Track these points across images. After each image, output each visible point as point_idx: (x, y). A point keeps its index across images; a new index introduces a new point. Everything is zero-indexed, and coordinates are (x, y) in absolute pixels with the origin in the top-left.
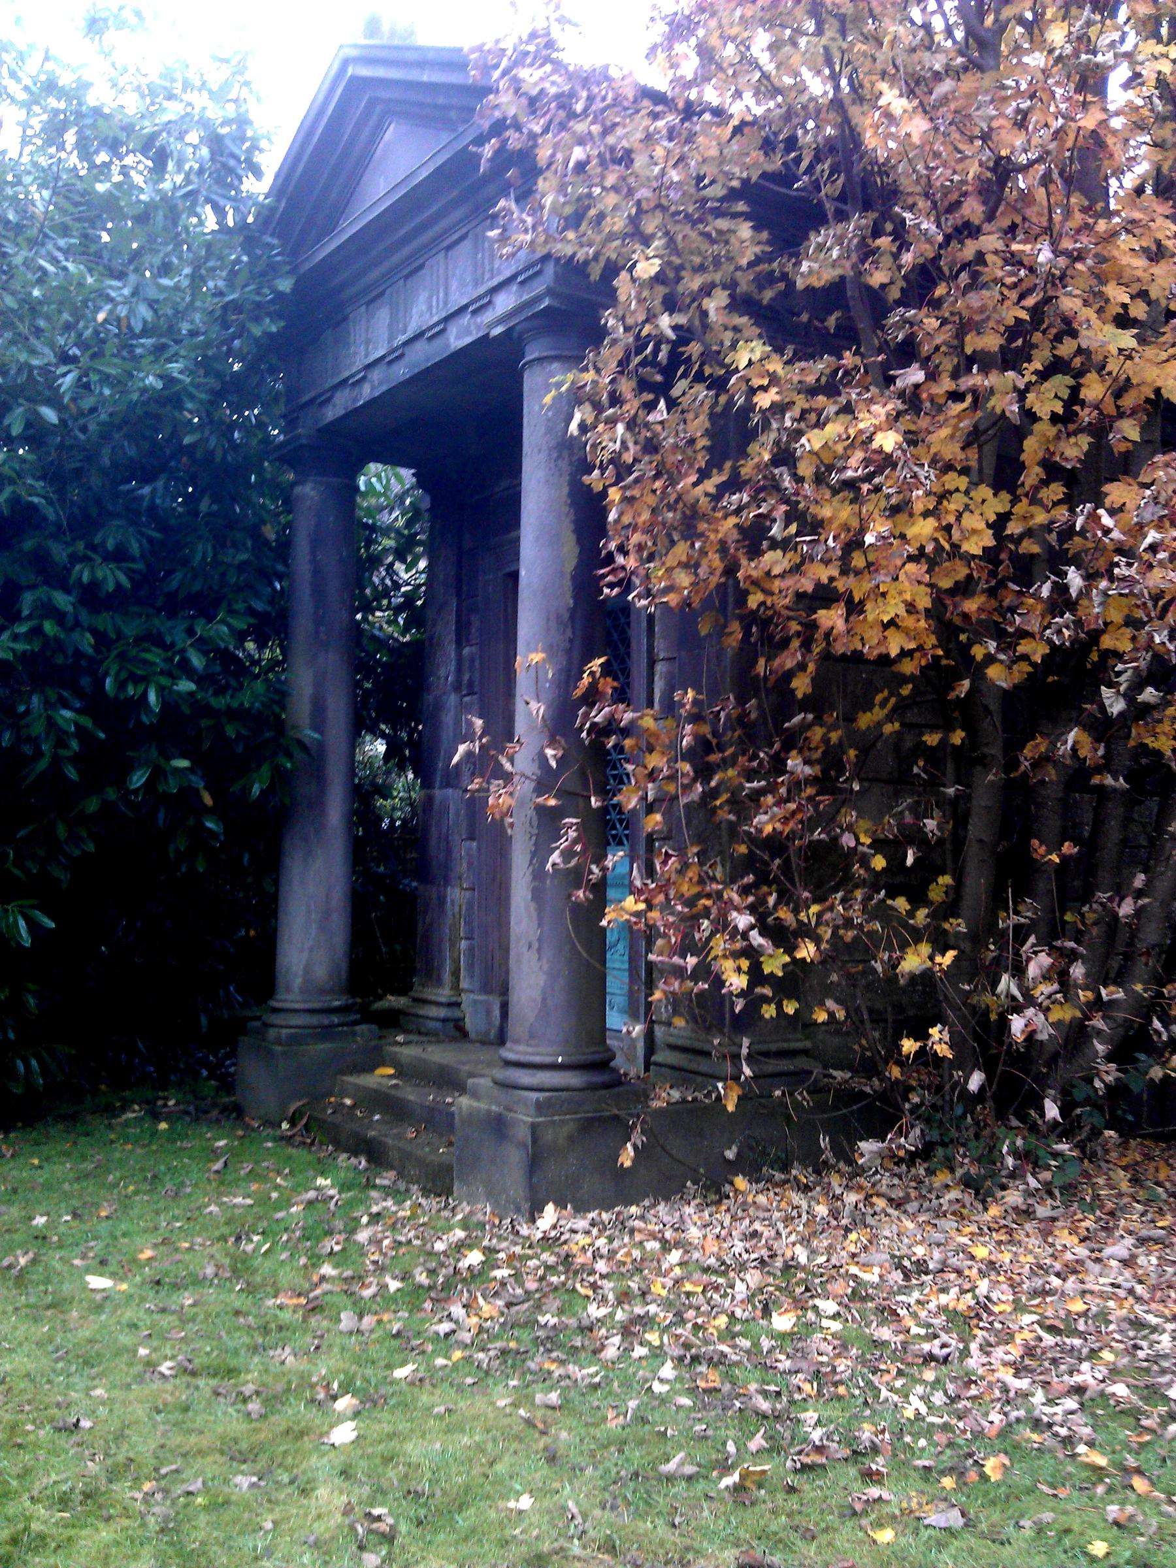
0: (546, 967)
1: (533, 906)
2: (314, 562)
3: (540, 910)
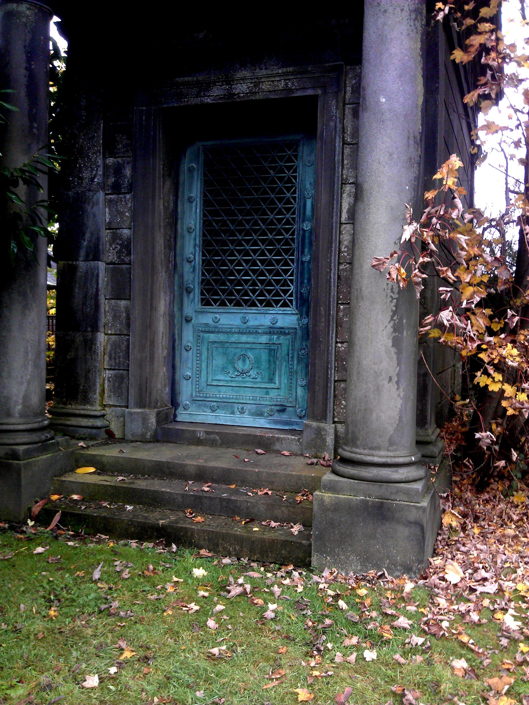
0: (402, 394)
1: (393, 350)
2: (28, 69)
3: (399, 353)
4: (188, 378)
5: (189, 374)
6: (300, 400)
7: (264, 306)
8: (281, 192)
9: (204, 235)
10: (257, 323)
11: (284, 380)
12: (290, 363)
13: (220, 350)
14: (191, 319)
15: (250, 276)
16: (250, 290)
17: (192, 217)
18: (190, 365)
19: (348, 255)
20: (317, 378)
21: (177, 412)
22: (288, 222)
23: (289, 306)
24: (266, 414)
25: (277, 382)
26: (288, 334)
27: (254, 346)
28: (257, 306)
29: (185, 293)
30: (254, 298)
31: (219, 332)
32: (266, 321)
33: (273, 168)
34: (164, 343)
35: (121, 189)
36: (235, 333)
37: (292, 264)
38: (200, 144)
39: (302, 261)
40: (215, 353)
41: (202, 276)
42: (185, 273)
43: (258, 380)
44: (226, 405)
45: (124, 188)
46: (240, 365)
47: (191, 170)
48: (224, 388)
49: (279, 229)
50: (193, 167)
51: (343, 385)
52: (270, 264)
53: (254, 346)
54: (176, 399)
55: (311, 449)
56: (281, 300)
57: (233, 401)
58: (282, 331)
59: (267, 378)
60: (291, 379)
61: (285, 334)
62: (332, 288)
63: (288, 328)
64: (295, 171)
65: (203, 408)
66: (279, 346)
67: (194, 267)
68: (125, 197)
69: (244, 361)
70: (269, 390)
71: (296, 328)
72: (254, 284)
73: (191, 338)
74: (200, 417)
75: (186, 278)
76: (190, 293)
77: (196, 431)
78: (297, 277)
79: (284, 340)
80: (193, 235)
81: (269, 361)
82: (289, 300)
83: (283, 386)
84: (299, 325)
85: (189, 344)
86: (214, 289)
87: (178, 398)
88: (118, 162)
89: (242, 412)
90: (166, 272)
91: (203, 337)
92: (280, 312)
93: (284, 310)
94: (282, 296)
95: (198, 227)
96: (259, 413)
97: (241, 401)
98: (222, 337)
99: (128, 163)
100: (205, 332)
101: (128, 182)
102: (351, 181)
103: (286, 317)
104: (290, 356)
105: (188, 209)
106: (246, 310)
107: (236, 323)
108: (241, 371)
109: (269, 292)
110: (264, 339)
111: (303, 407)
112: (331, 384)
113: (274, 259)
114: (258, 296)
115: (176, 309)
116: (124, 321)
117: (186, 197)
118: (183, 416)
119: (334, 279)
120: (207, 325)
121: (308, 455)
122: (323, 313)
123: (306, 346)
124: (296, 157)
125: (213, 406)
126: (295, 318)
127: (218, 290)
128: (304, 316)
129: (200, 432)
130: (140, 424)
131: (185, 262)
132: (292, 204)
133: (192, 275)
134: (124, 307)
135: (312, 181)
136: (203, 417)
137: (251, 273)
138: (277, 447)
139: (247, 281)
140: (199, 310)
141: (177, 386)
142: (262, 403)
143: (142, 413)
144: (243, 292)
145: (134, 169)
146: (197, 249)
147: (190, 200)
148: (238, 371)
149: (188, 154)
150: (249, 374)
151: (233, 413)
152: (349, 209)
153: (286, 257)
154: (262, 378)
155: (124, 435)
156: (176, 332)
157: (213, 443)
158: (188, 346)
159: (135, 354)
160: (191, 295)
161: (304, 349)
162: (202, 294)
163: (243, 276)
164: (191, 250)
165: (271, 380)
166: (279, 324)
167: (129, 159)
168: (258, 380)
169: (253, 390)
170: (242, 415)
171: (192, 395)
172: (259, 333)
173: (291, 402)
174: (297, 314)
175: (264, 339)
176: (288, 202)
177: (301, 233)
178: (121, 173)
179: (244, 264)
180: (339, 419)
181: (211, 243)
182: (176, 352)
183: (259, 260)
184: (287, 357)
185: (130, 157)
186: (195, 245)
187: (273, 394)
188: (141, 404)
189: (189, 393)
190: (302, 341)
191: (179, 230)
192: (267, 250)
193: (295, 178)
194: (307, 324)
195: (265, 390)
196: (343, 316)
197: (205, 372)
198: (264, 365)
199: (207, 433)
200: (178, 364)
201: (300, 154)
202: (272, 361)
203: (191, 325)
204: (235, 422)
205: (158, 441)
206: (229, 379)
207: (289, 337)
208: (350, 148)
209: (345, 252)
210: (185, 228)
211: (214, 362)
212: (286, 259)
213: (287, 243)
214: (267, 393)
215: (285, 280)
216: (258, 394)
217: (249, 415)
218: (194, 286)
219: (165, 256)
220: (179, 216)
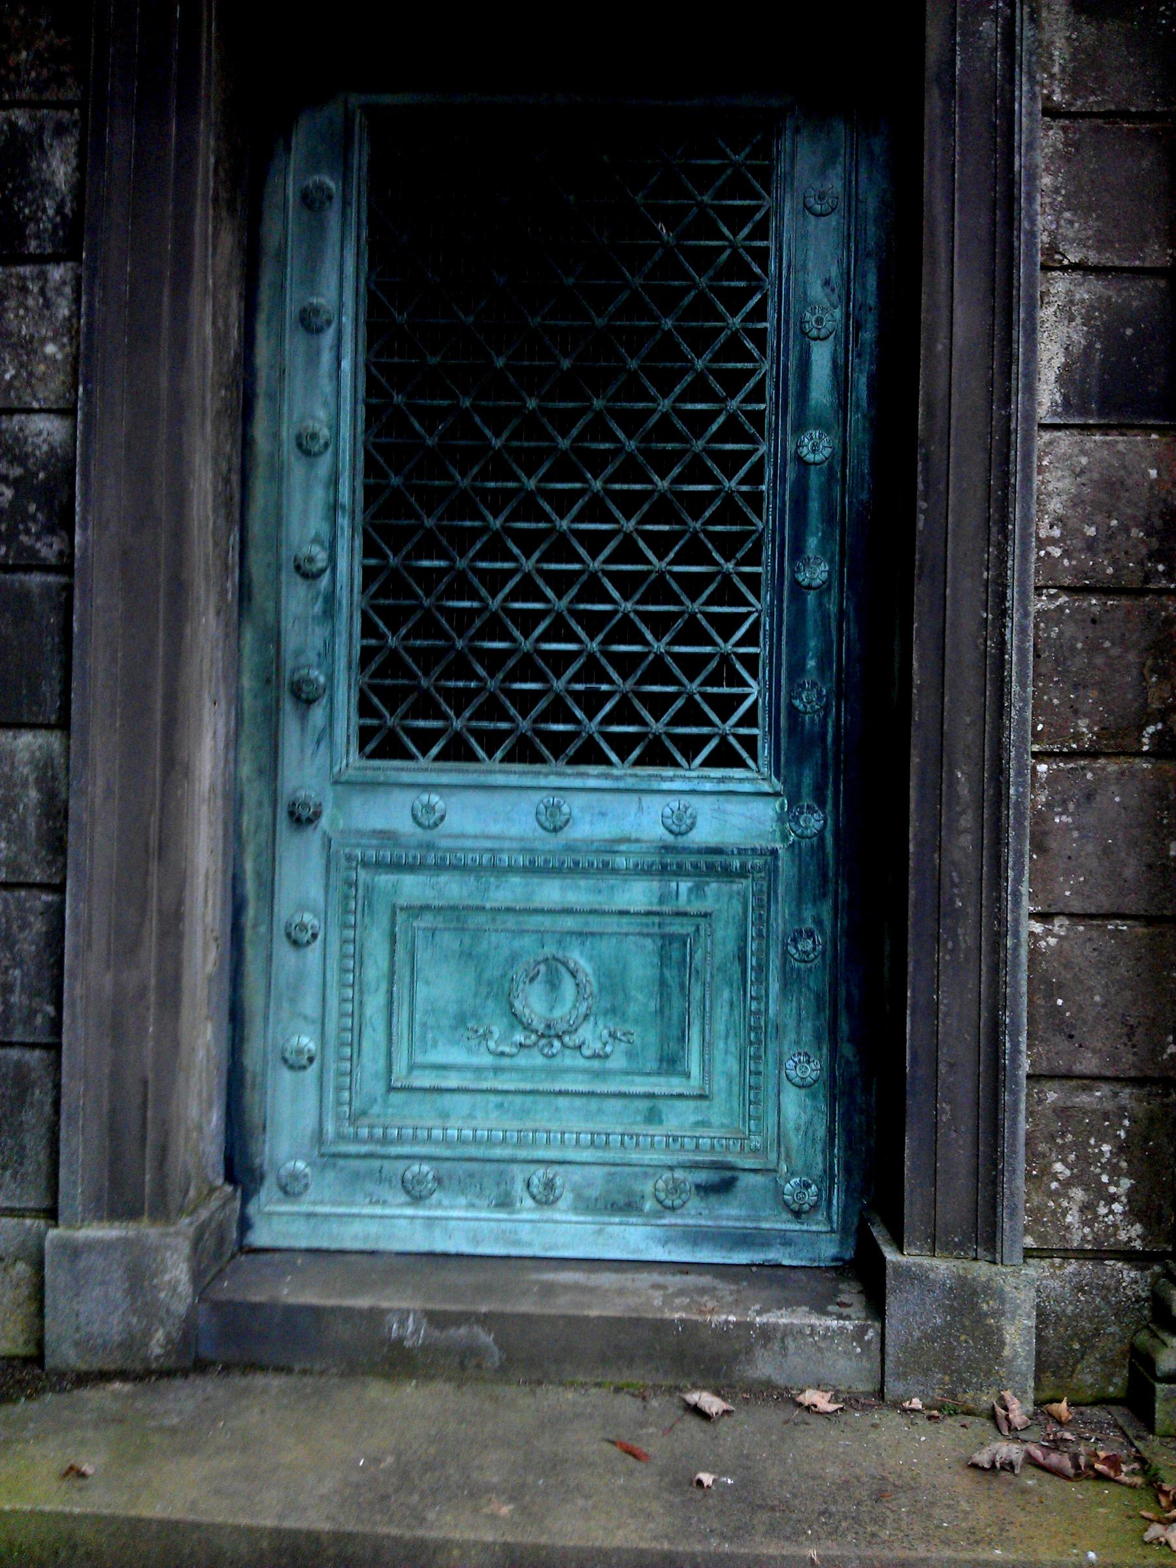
4: (296, 1064)
5: (307, 1042)
6: (795, 1140)
7: (639, 762)
8: (701, 307)
9: (371, 467)
10: (604, 830)
11: (726, 1063)
12: (752, 990)
13: (448, 940)
14: (317, 815)
15: (573, 638)
16: (575, 695)
17: (321, 393)
18: (309, 1004)
19: (1066, 553)
20: (943, 1069)
21: (252, 1209)
22: (732, 430)
23: (742, 764)
24: (648, 1205)
25: (695, 1070)
26: (743, 873)
27: (595, 923)
28: (608, 762)
29: (288, 705)
30: (593, 726)
31: (440, 867)
32: (645, 820)
33: (672, 218)
34: (209, 919)
35: (23, 240)
36: (511, 869)
37: (751, 598)
38: (355, 100)
39: (795, 583)
40: (423, 956)
41: (365, 634)
42: (287, 624)
43: (611, 1064)
44: (480, 1173)
45: (37, 236)
46: (534, 1003)
47: (312, 201)
48: (466, 1098)
49: (697, 457)
50: (320, 187)
51: (1052, 1096)
52: (659, 590)
53: (595, 923)
54: (245, 1153)
55: (926, 1372)
56: (707, 739)
57: (506, 1152)
58: (714, 864)
59: (652, 1053)
60: (757, 1058)
61: (727, 873)
62: (1015, 688)
63: (741, 852)
64: (761, 231)
65: (369, 1186)
66: (702, 922)
67: (330, 599)
68: (43, 276)
69: (553, 985)
70: (662, 1105)
71: (774, 852)
72: (592, 670)
73: (315, 891)
74: (357, 1227)
75: (291, 640)
76: (309, 702)
77: (383, 1312)
78: (775, 649)
79: (720, 899)
80: (324, 465)
81: (663, 983)
82: (738, 737)
83: (719, 1083)
84: (785, 837)
85: (308, 918)
86: (418, 687)
87: (253, 1148)
88: (12, 125)
89: (546, 1197)
90: (218, 613)
91: (370, 889)
92: (708, 786)
93: (722, 780)
94: (711, 724)
95: (346, 431)
96: (621, 1200)
97: (540, 1154)
98: (453, 889)
99: (60, 130)
100: (379, 865)
101: (59, 209)
102: (1073, 258)
103: (734, 807)
104: (752, 961)
105: (300, 361)
106: (554, 776)
107: (514, 831)
108: (541, 1028)
109: (657, 705)
110: (638, 894)
111: (808, 1167)
112: (1015, 1093)
113: (677, 576)
114: (607, 720)
115: (246, 770)
116: (32, 823)
117: (292, 309)
118: (278, 1225)
119: (1022, 652)
120: (387, 836)
121: (917, 1403)
122: (964, 791)
123: (818, 922)
124: (766, 176)
125: (419, 1179)
126: (767, 811)
127: (437, 688)
128: (806, 801)
129: (403, 1316)
130: (117, 1294)
131: (288, 576)
132: (752, 359)
133: (322, 632)
134: (32, 760)
135: (834, 271)
136: (373, 1228)
137: (579, 630)
138: (764, 1367)
139: (560, 661)
140: (351, 774)
141: (251, 1098)
142: (634, 1156)
143: (126, 1241)
144: (542, 705)
145: (89, 159)
146: (344, 522)
147: (310, 322)
148: (527, 1028)
149: (299, 139)
150: (576, 1039)
151: (505, 1203)
152: (1066, 367)
153: (730, 566)
154: (630, 1055)
155: (40, 1344)
156: (249, 866)
157: (463, 1365)
158: (303, 927)
159: (88, 977)
160: (318, 714)
161: (810, 934)
162: (365, 708)
163: (546, 637)
164: (317, 524)
165: (671, 1063)
166: (704, 834)
167: (64, 116)
168: (611, 1064)
169: (594, 1104)
170: (548, 1214)
171: (319, 1135)
172: (615, 871)
173: (755, 1151)
174: (776, 794)
175: (638, 894)
176: (733, 349)
177: (791, 474)
178: (26, 171)
179: (549, 593)
180: (1040, 1237)
181: (403, 496)
182: (250, 952)
183: (614, 577)
184: (736, 969)
185: (68, 106)
186: (334, 508)
187: (679, 1119)
188: (119, 1201)
189: (309, 1122)
190: (799, 901)
191: (262, 443)
192: (648, 537)
193: (762, 256)
194: (821, 834)
195: (644, 1105)
196: (1049, 805)
197: (380, 1036)
198: (641, 1001)
199: (437, 1319)
200: (254, 998)
201: (782, 167)
202: (673, 982)
203: (313, 839)
204: (517, 1243)
205: (201, 1367)
206: (487, 1060)
207: (744, 884)
208: (1065, 129)
209: (1053, 541)
210: (287, 434)
211: (421, 991)
212: (727, 577)
213: (729, 511)
214: (653, 1117)
215: (725, 658)
216: (614, 1120)
217: (575, 1209)
218: (330, 677)
219: (216, 544)
220: (262, 387)
